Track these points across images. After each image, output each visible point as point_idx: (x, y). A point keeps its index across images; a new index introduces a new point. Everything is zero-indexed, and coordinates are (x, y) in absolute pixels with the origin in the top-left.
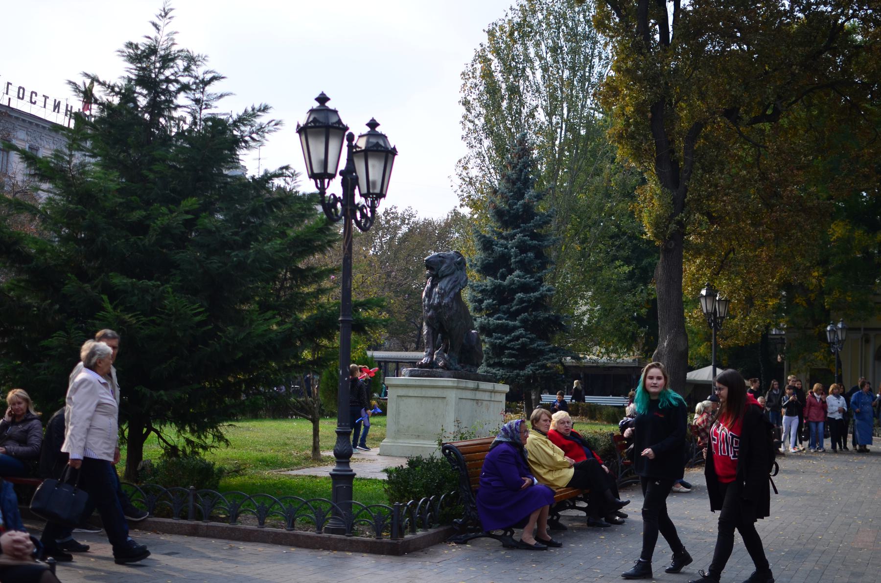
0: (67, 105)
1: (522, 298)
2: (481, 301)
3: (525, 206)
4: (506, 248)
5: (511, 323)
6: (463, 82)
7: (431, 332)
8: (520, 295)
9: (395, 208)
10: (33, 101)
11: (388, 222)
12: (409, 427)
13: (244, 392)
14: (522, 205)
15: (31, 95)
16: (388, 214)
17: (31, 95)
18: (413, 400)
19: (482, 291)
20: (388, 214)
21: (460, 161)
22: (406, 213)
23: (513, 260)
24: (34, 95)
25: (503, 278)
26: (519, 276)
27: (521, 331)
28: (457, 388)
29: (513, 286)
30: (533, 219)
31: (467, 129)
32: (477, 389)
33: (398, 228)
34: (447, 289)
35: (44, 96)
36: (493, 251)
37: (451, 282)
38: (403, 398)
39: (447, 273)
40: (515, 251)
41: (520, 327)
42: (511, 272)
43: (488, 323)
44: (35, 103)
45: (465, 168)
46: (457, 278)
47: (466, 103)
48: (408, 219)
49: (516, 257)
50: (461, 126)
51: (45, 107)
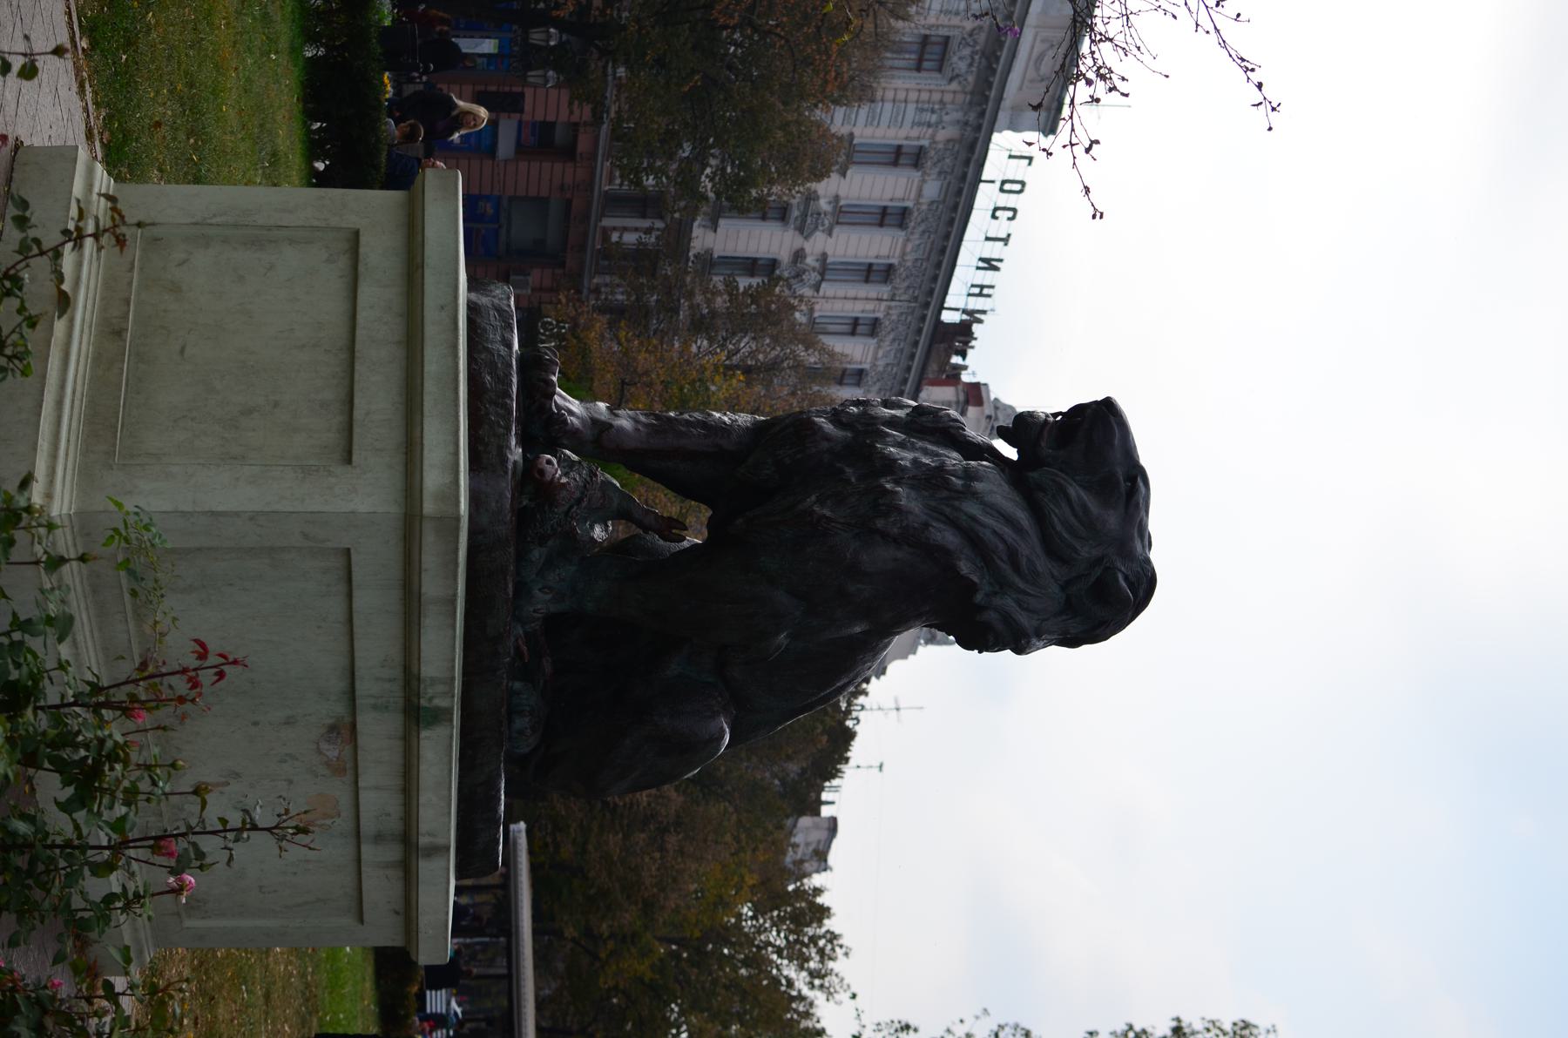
0: (984, 312)
9: (846, 954)
10: (998, 213)
11: (814, 940)
12: (175, 289)
15: (1009, 209)
16: (830, 941)
17: (1009, 209)
20: (830, 941)
22: (836, 980)
24: (1010, 214)
28: (410, 523)
32: (415, 715)
33: (802, 961)
34: (972, 508)
35: (1009, 235)
37: (1007, 531)
38: (343, 262)
44: (994, 217)
48: (822, 986)
51: (988, 239)
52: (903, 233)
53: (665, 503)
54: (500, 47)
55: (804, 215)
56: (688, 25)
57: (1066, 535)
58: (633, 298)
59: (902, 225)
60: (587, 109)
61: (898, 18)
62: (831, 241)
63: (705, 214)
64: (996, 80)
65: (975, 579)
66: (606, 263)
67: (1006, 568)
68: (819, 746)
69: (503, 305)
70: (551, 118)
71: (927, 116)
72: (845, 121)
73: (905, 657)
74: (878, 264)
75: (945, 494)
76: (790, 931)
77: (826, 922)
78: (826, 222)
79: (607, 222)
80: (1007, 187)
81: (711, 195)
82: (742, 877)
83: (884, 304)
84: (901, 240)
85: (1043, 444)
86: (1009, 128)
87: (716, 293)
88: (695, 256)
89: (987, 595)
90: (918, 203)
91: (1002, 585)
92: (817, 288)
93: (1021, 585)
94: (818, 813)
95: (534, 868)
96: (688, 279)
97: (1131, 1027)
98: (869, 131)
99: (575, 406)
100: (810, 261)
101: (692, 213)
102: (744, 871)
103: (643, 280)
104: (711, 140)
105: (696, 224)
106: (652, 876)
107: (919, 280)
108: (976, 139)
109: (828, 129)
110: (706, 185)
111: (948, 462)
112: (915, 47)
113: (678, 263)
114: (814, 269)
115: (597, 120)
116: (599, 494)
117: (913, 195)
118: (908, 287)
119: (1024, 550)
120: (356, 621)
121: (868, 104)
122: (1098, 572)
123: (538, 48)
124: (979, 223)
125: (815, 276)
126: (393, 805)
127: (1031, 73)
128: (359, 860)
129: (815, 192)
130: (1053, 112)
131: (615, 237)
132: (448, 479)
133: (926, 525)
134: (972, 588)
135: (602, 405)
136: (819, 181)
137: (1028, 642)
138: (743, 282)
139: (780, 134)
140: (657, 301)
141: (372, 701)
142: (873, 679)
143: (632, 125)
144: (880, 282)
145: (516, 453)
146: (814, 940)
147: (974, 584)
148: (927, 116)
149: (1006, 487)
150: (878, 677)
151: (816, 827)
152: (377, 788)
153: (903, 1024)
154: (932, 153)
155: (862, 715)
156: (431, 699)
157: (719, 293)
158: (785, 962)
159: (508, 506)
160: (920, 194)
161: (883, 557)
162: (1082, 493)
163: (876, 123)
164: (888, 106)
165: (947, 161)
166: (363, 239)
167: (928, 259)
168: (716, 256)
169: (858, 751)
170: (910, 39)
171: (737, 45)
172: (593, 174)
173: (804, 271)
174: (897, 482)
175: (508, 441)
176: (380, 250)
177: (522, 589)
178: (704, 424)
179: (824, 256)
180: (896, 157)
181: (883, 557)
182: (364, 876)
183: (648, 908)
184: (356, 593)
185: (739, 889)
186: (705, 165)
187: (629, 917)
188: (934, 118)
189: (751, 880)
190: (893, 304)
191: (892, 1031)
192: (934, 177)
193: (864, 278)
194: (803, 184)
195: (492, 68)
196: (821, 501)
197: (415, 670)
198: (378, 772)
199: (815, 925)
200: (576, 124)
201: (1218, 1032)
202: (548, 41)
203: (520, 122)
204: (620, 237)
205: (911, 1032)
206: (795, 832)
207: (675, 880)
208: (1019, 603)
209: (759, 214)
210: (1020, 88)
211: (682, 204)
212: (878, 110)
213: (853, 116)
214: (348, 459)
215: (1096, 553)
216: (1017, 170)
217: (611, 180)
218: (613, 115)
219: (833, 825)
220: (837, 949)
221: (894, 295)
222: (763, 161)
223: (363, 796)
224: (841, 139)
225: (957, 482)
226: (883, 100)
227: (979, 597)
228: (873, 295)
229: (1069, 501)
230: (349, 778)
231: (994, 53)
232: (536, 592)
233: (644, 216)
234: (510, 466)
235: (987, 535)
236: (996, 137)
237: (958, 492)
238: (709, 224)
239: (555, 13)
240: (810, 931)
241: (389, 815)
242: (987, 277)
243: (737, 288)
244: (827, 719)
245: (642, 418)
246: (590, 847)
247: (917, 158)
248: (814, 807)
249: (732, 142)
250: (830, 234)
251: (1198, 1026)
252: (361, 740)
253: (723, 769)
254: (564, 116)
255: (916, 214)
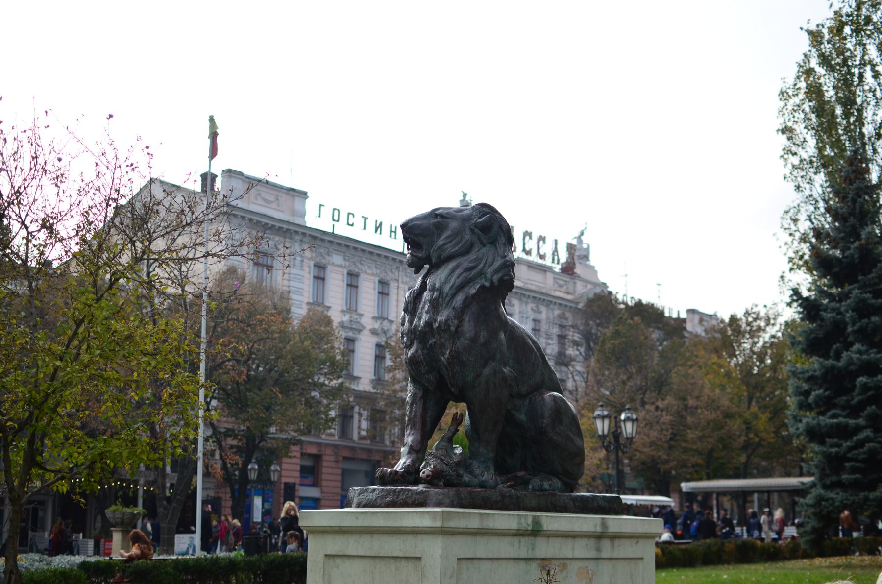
1: (866, 383)
2: (807, 394)
3: (861, 249)
4: (840, 313)
5: (852, 422)
6: (782, 104)
7: (420, 394)
8: (862, 379)
9: (756, 306)
11: (748, 324)
13: (284, 550)
14: (857, 248)
16: (749, 314)
18: (357, 565)
19: (810, 379)
20: (749, 314)
21: (787, 212)
23: (850, 329)
24: (351, 216)
25: (838, 357)
26: (860, 352)
27: (867, 433)
28: (444, 532)
29: (852, 368)
30: (875, 266)
31: (790, 166)
32: (536, 532)
34: (447, 288)
36: (822, 320)
37: (458, 272)
38: (338, 561)
39: (450, 249)
40: (851, 317)
41: (865, 427)
42: (848, 346)
43: (819, 424)
44: (352, 225)
45: (795, 221)
46: (478, 260)
47: (786, 130)
48: (774, 319)
49: (854, 324)
50: (782, 161)
52: (361, 275)
53: (446, 420)
54: (258, 495)
55: (352, 329)
56: (248, 393)
57: (460, 246)
58: (397, 423)
59: (357, 276)
60: (293, 448)
61: (244, 279)
62: (366, 315)
63: (350, 384)
64: (278, 225)
65: (478, 286)
66: (378, 438)
67: (474, 272)
68: (640, 322)
69: (357, 492)
70: (298, 468)
71: (298, 262)
72: (299, 311)
73: (596, 272)
74: (379, 288)
75: (440, 300)
76: (744, 336)
77: (739, 317)
78: (356, 317)
79: (355, 437)
80: (336, 218)
81: (340, 380)
82: (714, 363)
83: (401, 285)
84: (365, 276)
85: (420, 255)
86: (304, 218)
87: (394, 377)
88: (374, 389)
89: (486, 280)
90: (345, 267)
91: (481, 274)
92: (391, 322)
93: (481, 265)
94: (684, 321)
95: (709, 478)
96: (386, 393)
97: (782, 156)
98: (306, 294)
99: (402, 461)
100: (377, 326)
101: (349, 391)
102: (709, 362)
103: (387, 418)
104: (310, 380)
105: (357, 389)
106: (711, 414)
107: (387, 266)
108: (310, 235)
109: (305, 316)
110: (335, 383)
111: (428, 298)
112: (260, 269)
113: (377, 398)
114: (381, 324)
115: (299, 443)
116: (440, 451)
117: (341, 270)
118: (391, 272)
119: (466, 264)
120: (492, 557)
121: (291, 294)
122: (477, 230)
123: (259, 475)
124: (356, 233)
125: (385, 323)
126: (581, 543)
127: (274, 206)
128: (610, 559)
129: (339, 323)
130: (295, 194)
131: (364, 433)
132: (427, 516)
133: (454, 308)
134: (483, 287)
135: (402, 449)
136: (333, 321)
137: (508, 261)
138: (388, 363)
139: (306, 343)
140: (399, 410)
141: (530, 550)
142: (609, 289)
143: (302, 424)
144: (388, 287)
145: (421, 487)
146: (748, 324)
147: (480, 286)
148: (298, 262)
149: (439, 272)
150: (608, 287)
151: (692, 321)
152: (573, 549)
153: (780, 279)
154: (318, 259)
155: (629, 296)
156: (528, 525)
157: (394, 376)
158: (761, 339)
159: (441, 491)
160: (340, 266)
161: (468, 327)
162: (441, 238)
163: (301, 290)
164: (292, 283)
165: (322, 251)
166: (329, 553)
167: (376, 261)
168: (374, 378)
169: (646, 298)
170: (256, 272)
171: (258, 366)
172: (327, 445)
173: (382, 329)
174: (435, 321)
175: (414, 490)
176: (334, 545)
177: (482, 485)
178: (411, 405)
179: (374, 318)
180: (320, 279)
181: (468, 327)
182: (618, 557)
183: (728, 415)
184: (478, 556)
185: (721, 367)
186: (323, 384)
187: (736, 425)
188: (299, 258)
189: (715, 358)
190: (400, 280)
191: (784, 285)
192: (330, 258)
193: (386, 297)
194: (334, 330)
195: (271, 500)
196: (444, 354)
197: (515, 531)
198: (566, 549)
199: (741, 323)
200: (302, 454)
201: (785, 109)
202: (255, 470)
203: (301, 485)
204: (364, 430)
205: (784, 275)
206: (695, 333)
207: (714, 401)
208: (489, 267)
209: (352, 353)
210: (282, 211)
211: (345, 396)
212: (294, 289)
213: (298, 302)
214: (419, 558)
215: (468, 232)
216: (327, 212)
217: (332, 435)
218: (296, 434)
219: (691, 312)
220: (754, 311)
221: (395, 279)
222: (321, 352)
223: (576, 556)
224: (309, 310)
225: (436, 294)
226: (289, 286)
227: (487, 284)
228: (395, 291)
229: (445, 244)
230: (568, 562)
231: (263, 226)
232: (483, 479)
233: (352, 417)
234: (424, 489)
235: (459, 281)
236: (308, 225)
237: (440, 294)
238: (356, 382)
239: (240, 466)
240: (744, 326)
241: (587, 545)
242: (386, 229)
243: (391, 366)
244: (624, 317)
245: (408, 432)
246: (695, 447)
247: (320, 267)
248: (681, 322)
249: (311, 369)
250: (362, 315)
251: (781, 120)
252: (549, 556)
253: (653, 374)
254: (297, 461)
255: (351, 268)
